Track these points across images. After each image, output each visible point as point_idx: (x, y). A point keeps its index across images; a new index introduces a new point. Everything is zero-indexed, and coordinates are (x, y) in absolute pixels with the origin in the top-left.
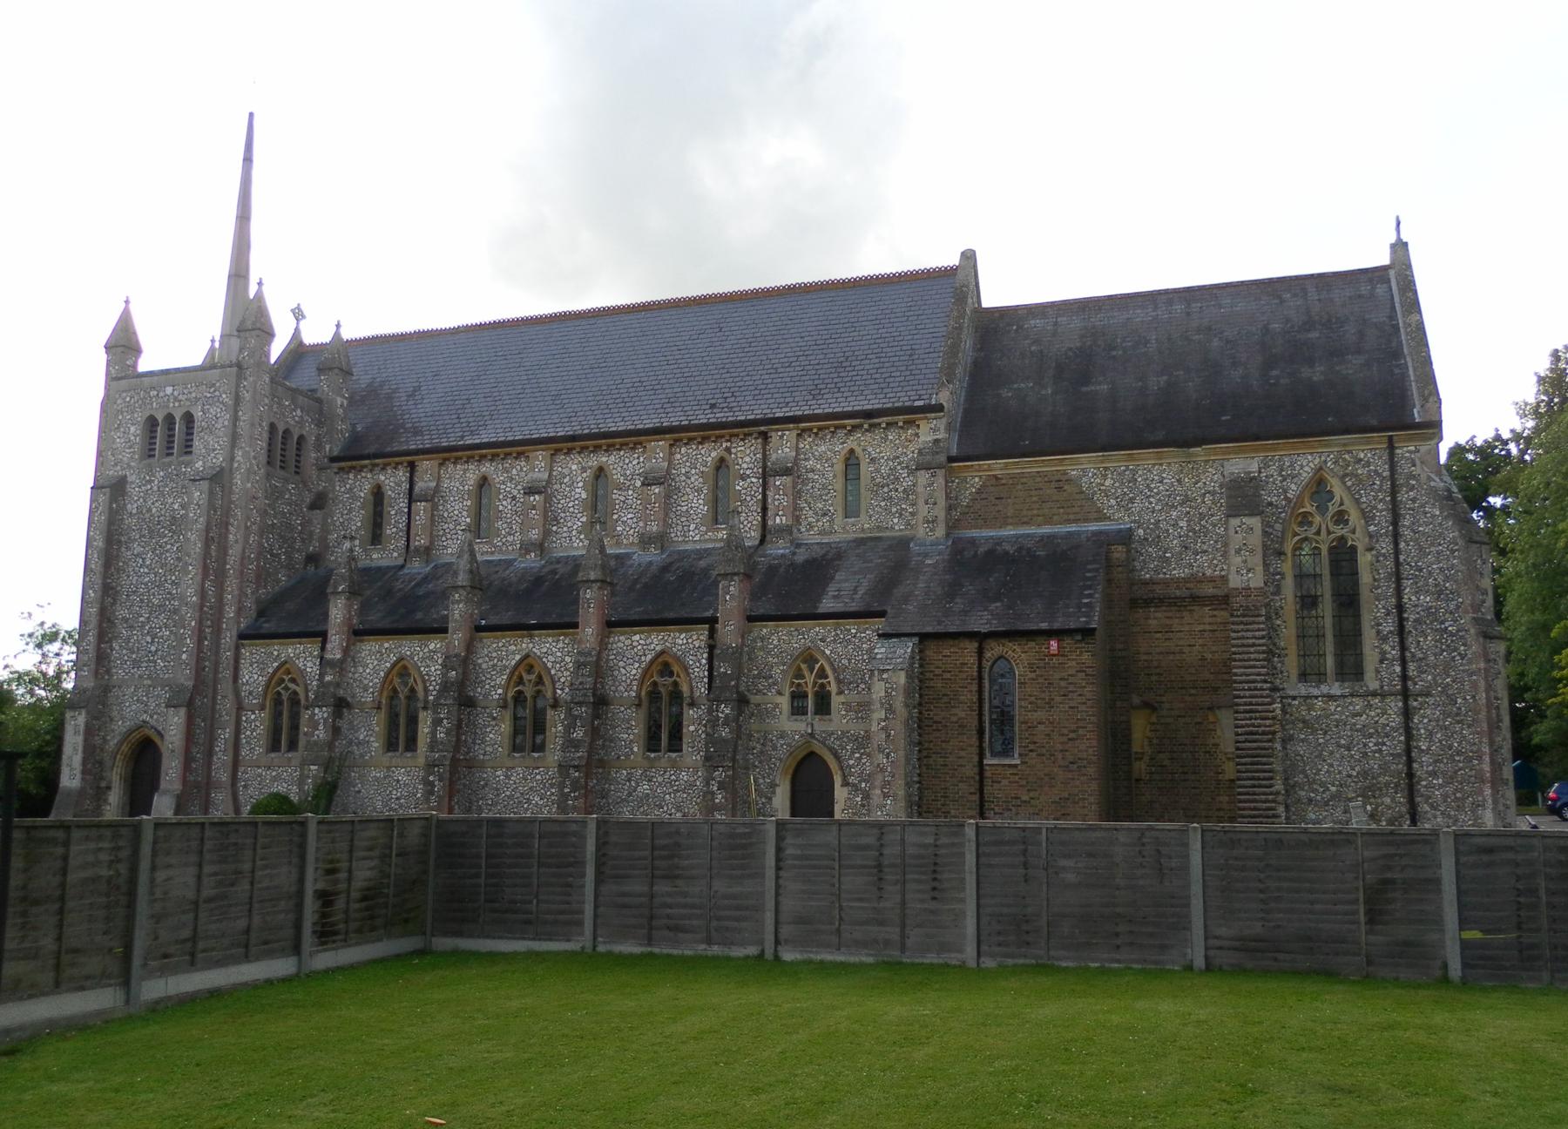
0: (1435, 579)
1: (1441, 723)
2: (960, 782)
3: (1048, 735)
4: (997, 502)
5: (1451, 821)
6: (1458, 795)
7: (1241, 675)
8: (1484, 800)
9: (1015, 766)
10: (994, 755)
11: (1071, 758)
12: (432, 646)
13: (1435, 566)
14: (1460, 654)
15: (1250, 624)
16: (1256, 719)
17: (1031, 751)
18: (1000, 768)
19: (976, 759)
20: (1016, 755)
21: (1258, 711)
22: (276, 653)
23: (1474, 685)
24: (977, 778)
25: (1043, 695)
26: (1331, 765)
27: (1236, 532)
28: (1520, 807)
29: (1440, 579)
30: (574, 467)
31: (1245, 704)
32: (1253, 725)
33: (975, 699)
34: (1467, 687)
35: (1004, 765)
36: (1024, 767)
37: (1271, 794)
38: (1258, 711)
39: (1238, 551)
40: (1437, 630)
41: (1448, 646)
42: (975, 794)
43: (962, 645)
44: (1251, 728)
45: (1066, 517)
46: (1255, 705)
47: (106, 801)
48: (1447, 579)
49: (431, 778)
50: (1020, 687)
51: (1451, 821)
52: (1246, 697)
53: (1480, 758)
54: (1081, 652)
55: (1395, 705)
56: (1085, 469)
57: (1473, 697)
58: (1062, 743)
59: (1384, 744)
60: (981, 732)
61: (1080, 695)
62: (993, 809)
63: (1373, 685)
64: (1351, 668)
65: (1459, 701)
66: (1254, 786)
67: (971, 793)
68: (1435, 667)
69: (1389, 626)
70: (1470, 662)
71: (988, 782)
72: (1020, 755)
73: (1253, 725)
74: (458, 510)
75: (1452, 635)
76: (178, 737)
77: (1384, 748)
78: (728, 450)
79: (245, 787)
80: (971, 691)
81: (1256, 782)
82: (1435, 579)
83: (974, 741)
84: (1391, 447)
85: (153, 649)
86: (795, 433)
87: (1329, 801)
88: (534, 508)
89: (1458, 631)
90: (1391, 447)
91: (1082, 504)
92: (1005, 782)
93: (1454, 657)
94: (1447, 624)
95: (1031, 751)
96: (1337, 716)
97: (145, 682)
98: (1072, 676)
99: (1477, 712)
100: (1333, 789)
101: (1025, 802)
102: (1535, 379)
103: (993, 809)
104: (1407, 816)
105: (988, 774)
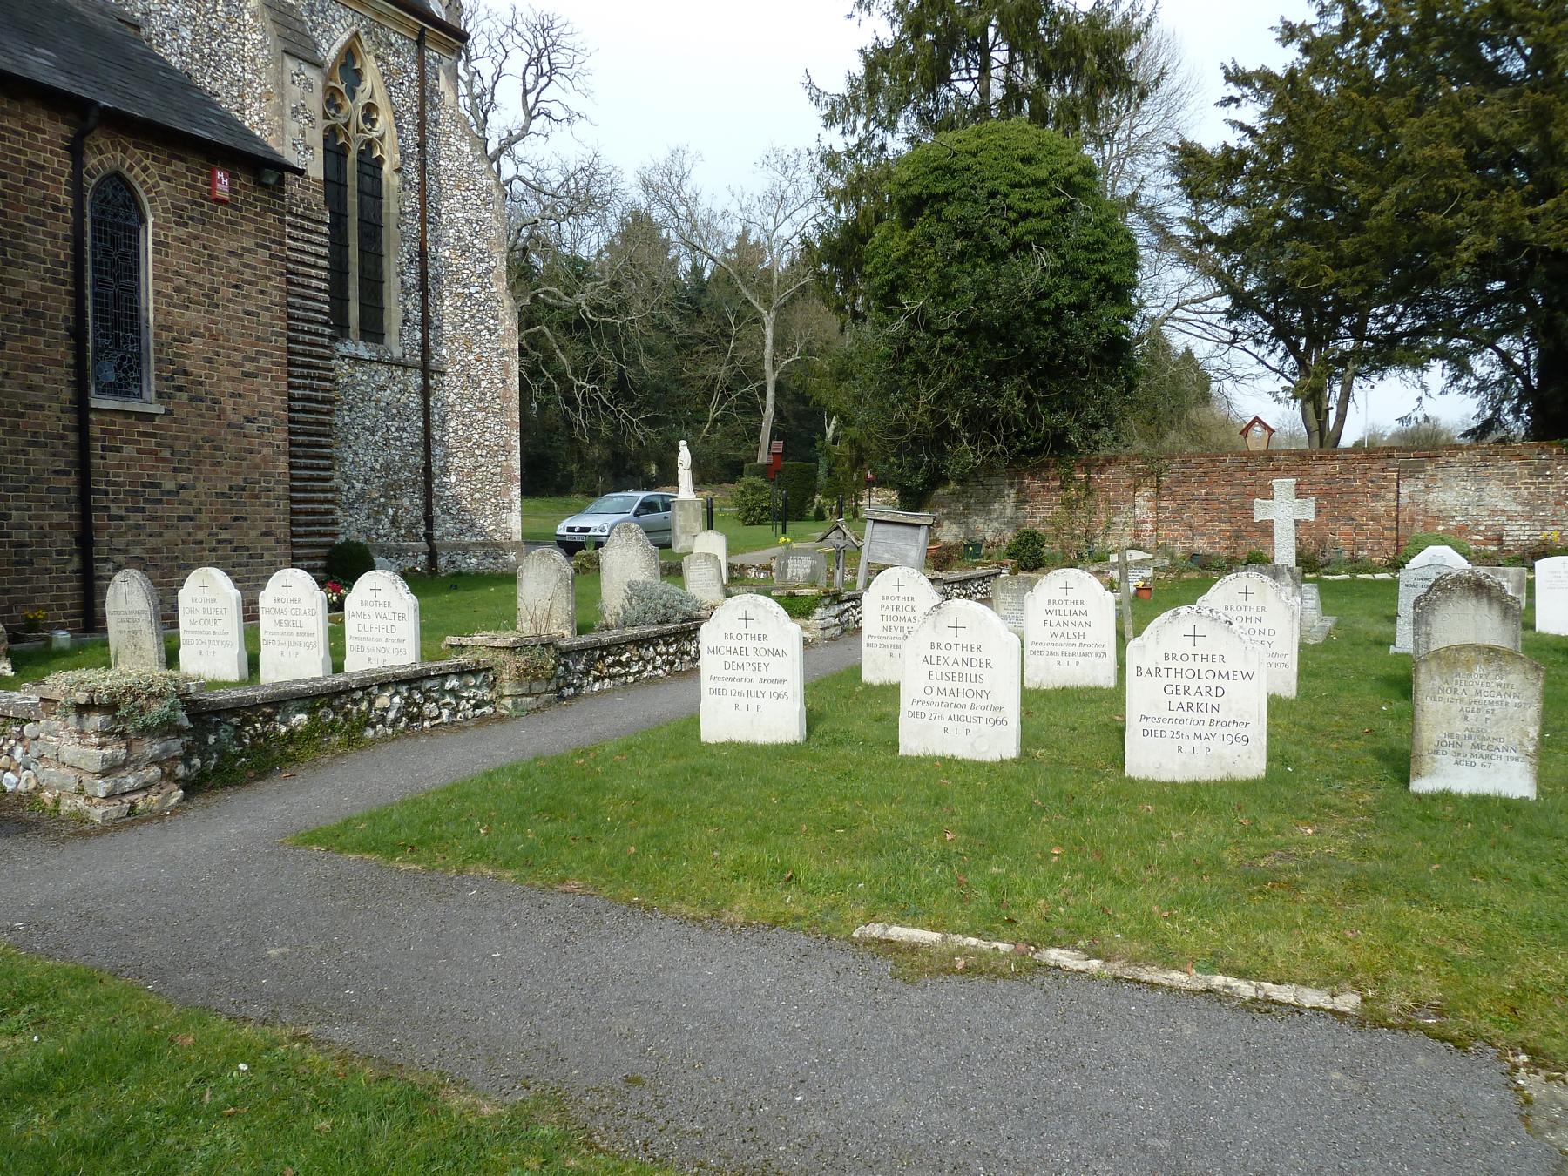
0: (459, 231)
2: (34, 444)
3: (210, 361)
6: (477, 495)
7: (298, 309)
8: (511, 501)
9: (150, 417)
10: (107, 389)
11: (247, 411)
13: (458, 215)
14: (488, 328)
15: (311, 232)
16: (312, 378)
17: (179, 388)
18: (119, 419)
19: (67, 394)
20: (150, 391)
21: (317, 368)
23: (506, 368)
24: (72, 437)
25: (199, 279)
26: (356, 454)
27: (293, 82)
28: (533, 502)
29: (466, 232)
31: (304, 354)
32: (311, 388)
33: (64, 253)
34: (496, 369)
35: (127, 414)
36: (165, 422)
37: (331, 491)
38: (317, 368)
39: (295, 112)
40: (457, 295)
41: (473, 317)
42: (66, 473)
43: (31, 119)
44: (307, 392)
46: (313, 357)
47: (32, 797)
50: (156, 252)
52: (303, 343)
54: (263, 209)
55: (415, 380)
57: (503, 381)
58: (232, 380)
59: (404, 430)
60: (77, 334)
61: (261, 292)
62: (107, 508)
63: (397, 352)
64: (373, 330)
65: (483, 384)
66: (312, 479)
67: (57, 472)
69: (411, 279)
70: (501, 339)
71: (97, 448)
72: (160, 395)
73: (311, 388)
75: (478, 303)
77: (405, 435)
80: (55, 236)
81: (315, 473)
82: (459, 231)
83: (63, 351)
87: (354, 502)
89: (487, 300)
92: (129, 450)
93: (480, 331)
94: (473, 290)
95: (179, 388)
96: (362, 388)
98: (249, 251)
99: (507, 400)
100: (358, 486)
101: (169, 493)
102: (1222, 74)
103: (107, 508)
104: (423, 522)
105: (95, 431)
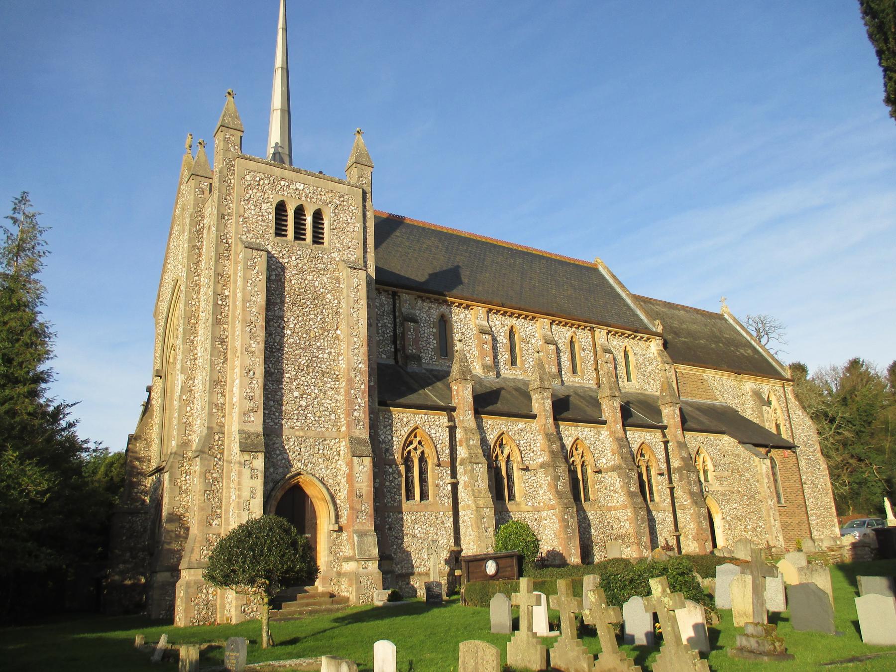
1: (812, 495)
4: (684, 385)
5: (821, 533)
12: (520, 426)
18: (782, 508)
22: (405, 420)
30: (497, 323)
45: (706, 397)
48: (808, 439)
49: (566, 517)
51: (821, 533)
53: (831, 508)
56: (710, 375)
68: (807, 473)
74: (429, 332)
76: (365, 484)
78: (574, 332)
79: (390, 529)
84: (783, 387)
85: (304, 403)
86: (606, 331)
88: (486, 343)
90: (783, 387)
91: (708, 389)
97: (297, 433)
